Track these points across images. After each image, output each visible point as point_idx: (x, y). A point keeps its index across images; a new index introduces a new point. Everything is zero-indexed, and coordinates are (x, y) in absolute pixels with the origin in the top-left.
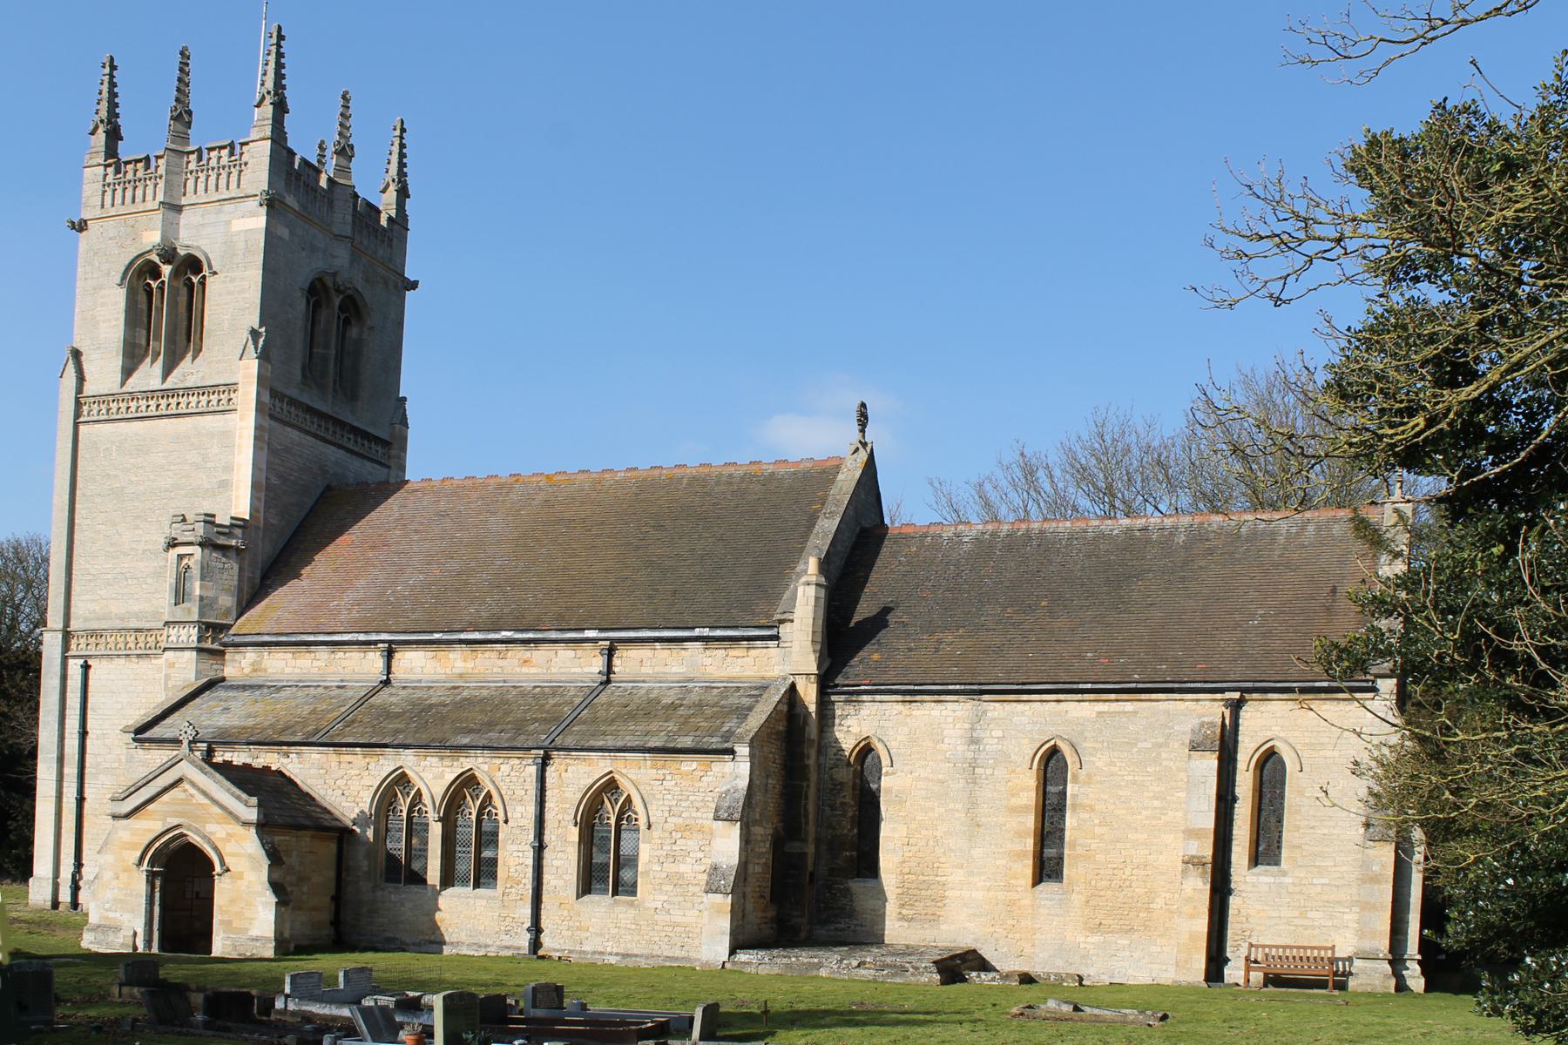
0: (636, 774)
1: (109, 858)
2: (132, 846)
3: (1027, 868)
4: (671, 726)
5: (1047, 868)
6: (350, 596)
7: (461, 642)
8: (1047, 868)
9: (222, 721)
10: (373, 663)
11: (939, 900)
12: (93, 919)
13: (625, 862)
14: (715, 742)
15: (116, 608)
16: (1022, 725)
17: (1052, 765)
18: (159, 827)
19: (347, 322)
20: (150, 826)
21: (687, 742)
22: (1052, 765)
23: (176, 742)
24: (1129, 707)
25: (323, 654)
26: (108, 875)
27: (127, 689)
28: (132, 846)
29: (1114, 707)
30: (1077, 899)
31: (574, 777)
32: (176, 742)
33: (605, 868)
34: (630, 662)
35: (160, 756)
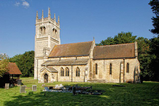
0: (79, 67)
1: (40, 75)
2: (42, 74)
3: (109, 73)
4: (82, 63)
5: (111, 73)
6: (57, 54)
7: (79, 56)
8: (111, 73)
9: (48, 64)
10: (59, 59)
11: (102, 76)
12: (39, 80)
13: (79, 74)
14: (85, 64)
15: (40, 55)
16: (108, 62)
17: (111, 65)
18: (44, 72)
19: (56, 32)
20: (43, 72)
21: (83, 64)
22: (111, 65)
23: (45, 66)
24: (116, 60)
25: (55, 58)
26: (40, 77)
27: (41, 62)
28: (42, 74)
29: (115, 60)
30: (113, 76)
31: (75, 67)
32: (45, 66)
33: (78, 74)
34: (77, 58)
35: (43, 67)
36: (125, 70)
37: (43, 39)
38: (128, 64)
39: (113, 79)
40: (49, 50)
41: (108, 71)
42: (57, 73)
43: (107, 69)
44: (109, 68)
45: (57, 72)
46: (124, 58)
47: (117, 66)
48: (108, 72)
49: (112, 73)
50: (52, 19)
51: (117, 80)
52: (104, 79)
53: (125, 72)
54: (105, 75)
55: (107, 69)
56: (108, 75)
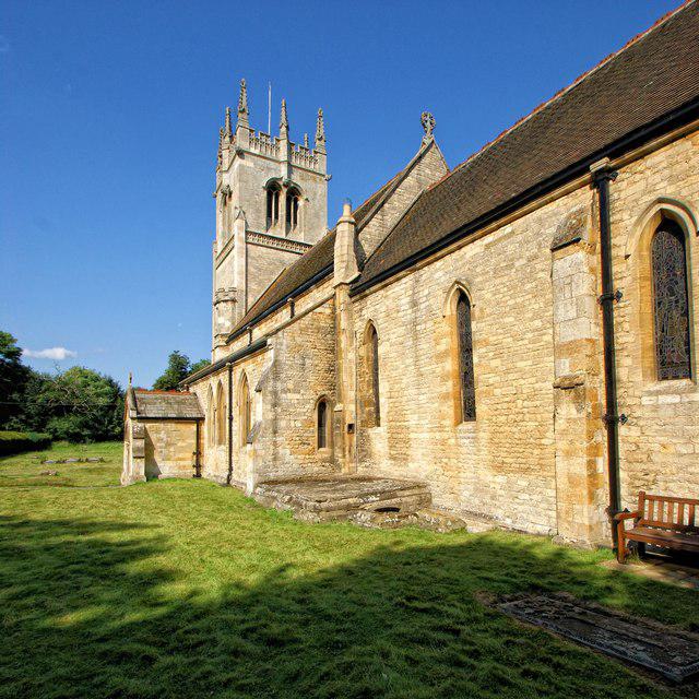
3: (450, 409)
5: (469, 412)
29: (500, 233)
36: (635, 335)
37: (227, 251)
38: (670, 226)
39: (488, 476)
40: (234, 301)
41: (444, 378)
42: (194, 427)
43: (561, 350)
44: (445, 354)
45: (199, 421)
46: (596, 165)
47: (519, 309)
48: (445, 397)
49: (481, 408)
50: (258, 133)
51: (529, 489)
52: (421, 477)
53: (622, 373)
54: (288, 452)
55: (561, 350)
56: (449, 422)
